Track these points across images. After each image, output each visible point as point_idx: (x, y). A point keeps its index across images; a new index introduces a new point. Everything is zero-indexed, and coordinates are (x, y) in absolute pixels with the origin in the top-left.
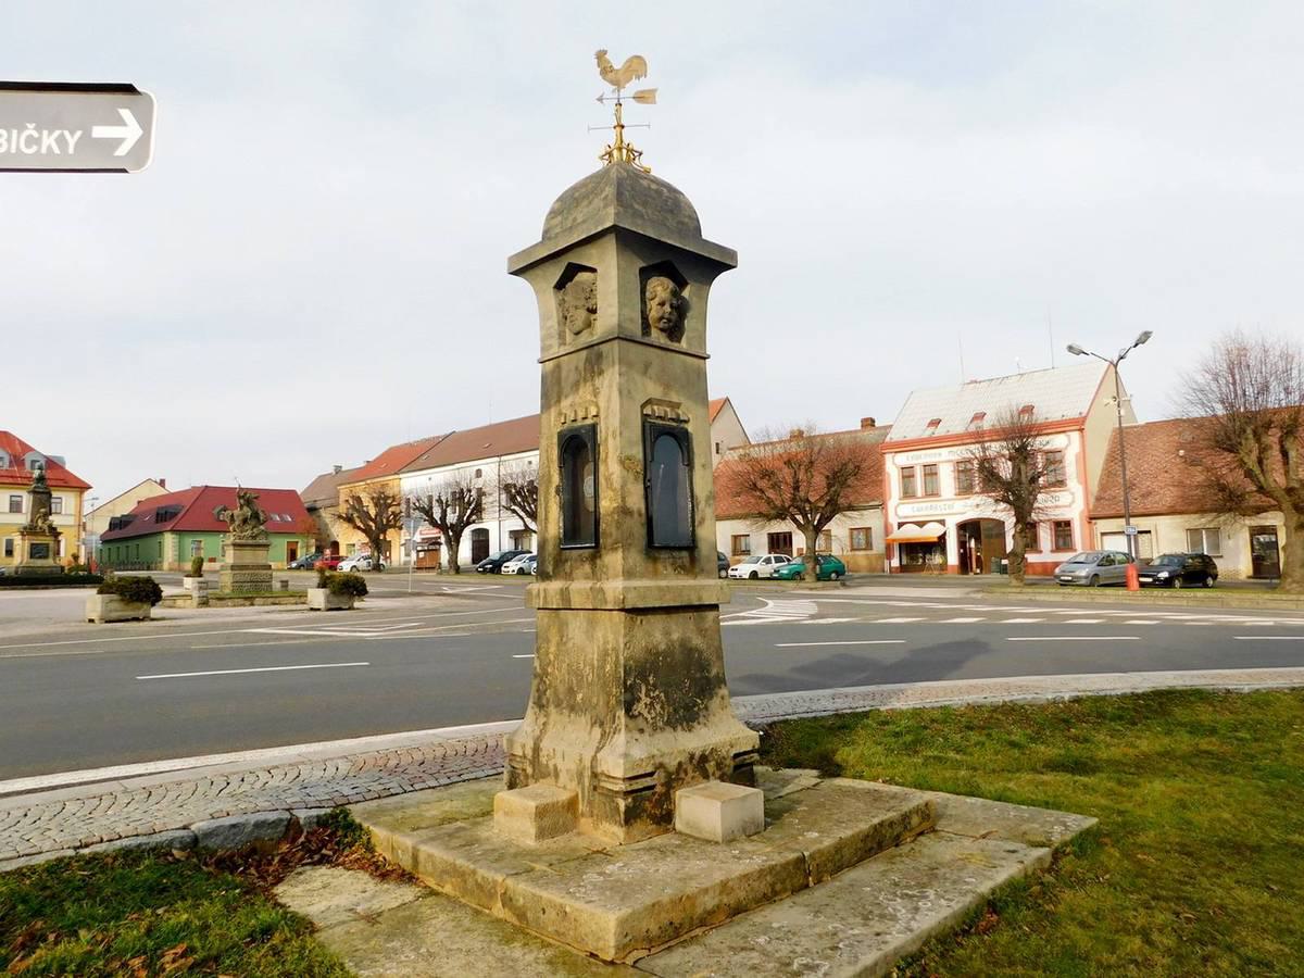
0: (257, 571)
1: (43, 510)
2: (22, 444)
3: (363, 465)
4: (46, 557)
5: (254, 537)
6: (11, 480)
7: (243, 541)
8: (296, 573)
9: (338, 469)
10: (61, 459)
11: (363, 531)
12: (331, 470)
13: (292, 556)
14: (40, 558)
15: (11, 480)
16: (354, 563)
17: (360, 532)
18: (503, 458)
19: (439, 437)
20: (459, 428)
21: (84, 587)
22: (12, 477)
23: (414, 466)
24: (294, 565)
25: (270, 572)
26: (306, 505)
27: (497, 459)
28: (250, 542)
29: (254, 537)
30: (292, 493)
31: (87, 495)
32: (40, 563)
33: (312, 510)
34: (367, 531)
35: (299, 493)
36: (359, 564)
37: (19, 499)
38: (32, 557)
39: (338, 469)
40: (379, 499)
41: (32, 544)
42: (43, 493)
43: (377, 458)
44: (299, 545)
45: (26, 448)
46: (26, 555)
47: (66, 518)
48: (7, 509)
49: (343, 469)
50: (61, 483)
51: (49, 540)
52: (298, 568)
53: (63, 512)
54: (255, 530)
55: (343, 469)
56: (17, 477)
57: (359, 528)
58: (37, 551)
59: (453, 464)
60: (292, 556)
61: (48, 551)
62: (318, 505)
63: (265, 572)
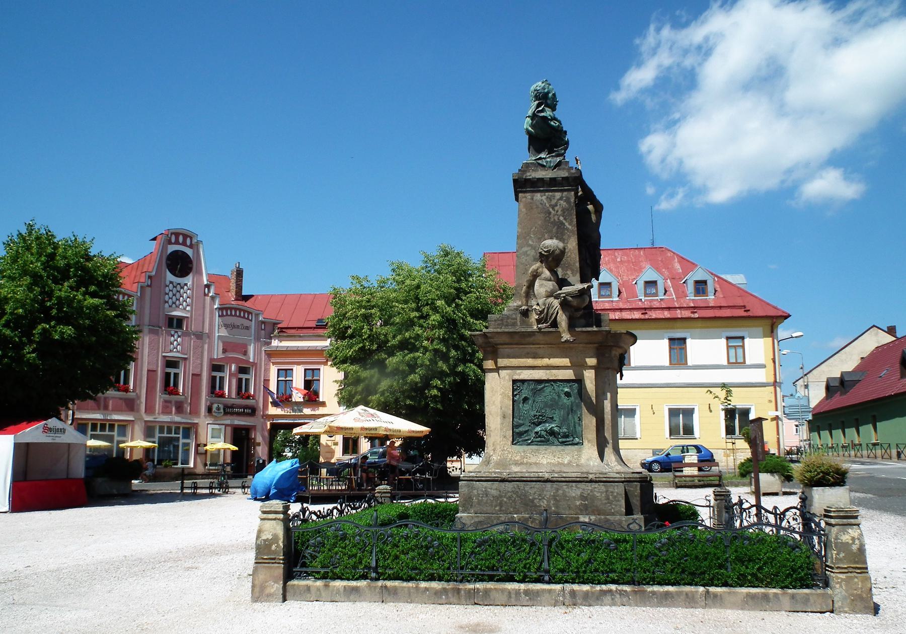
22: (669, 308)
50: (741, 313)
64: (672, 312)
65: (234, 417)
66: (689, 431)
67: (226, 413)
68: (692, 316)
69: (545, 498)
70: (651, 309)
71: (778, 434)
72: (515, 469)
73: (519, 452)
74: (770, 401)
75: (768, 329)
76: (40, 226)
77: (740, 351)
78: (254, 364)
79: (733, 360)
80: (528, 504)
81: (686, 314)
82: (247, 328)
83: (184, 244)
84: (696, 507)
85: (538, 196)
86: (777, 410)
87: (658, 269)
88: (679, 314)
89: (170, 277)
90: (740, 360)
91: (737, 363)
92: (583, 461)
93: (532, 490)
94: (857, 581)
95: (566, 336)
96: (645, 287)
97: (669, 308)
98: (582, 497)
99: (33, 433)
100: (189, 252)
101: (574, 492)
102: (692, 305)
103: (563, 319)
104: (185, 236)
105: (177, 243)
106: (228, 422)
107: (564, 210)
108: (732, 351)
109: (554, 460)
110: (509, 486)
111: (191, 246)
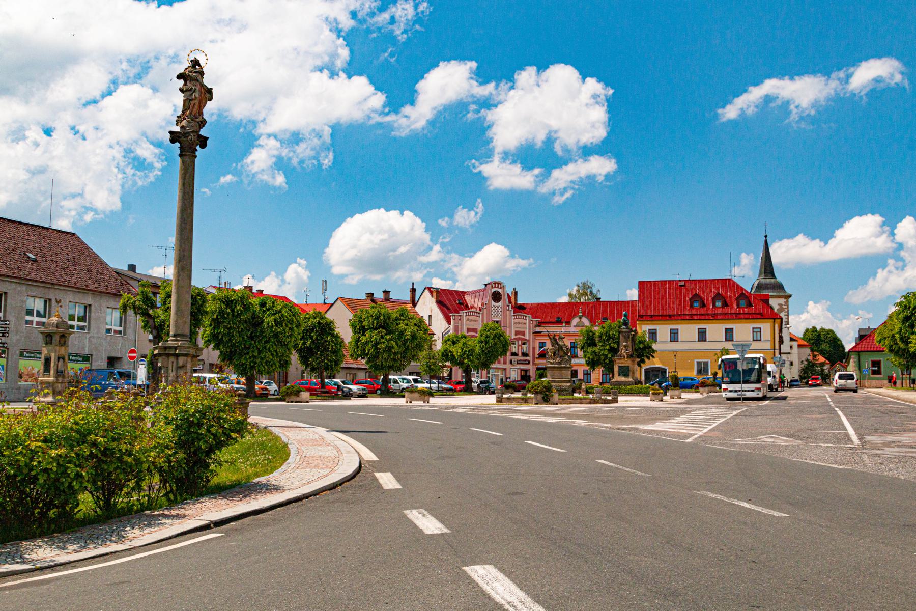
24: (142, 374)
53: (762, 339)
65: (521, 365)
67: (518, 363)
73: (619, 378)
76: (198, 58)
77: (759, 334)
78: (529, 341)
79: (755, 338)
82: (525, 324)
83: (498, 287)
84: (270, 428)
89: (493, 303)
90: (759, 338)
99: (173, 283)
100: (500, 291)
103: (626, 356)
104: (498, 284)
105: (495, 287)
106: (518, 367)
108: (755, 334)
111: (501, 288)
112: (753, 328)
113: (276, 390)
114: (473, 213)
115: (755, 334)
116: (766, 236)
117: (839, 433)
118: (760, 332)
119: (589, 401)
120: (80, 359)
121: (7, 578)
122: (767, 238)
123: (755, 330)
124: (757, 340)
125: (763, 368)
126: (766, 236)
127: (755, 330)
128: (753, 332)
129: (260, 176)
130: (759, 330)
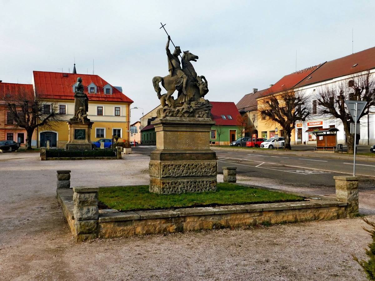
0: (195, 162)
1: (81, 108)
2: (103, 81)
3: (269, 87)
4: (84, 138)
5: (192, 114)
6: (97, 99)
7: (177, 119)
8: (236, 149)
9: (255, 90)
10: (120, 88)
11: (279, 122)
12: (252, 91)
13: (233, 138)
14: (80, 139)
15: (97, 99)
16: (270, 143)
17: (277, 123)
18: (371, 71)
19: (316, 66)
20: (329, 60)
21: (103, 159)
22: (98, 97)
23: (301, 84)
24: (234, 143)
25: (213, 162)
26: (239, 111)
27: (366, 72)
28: (186, 120)
29: (192, 114)
30: (232, 104)
31: (132, 106)
32: (80, 142)
33: (243, 113)
34: (282, 122)
35: (236, 104)
36: (273, 144)
37: (101, 109)
38: (75, 138)
39: (255, 90)
40: (289, 100)
41: (75, 130)
42: (81, 97)
43: (276, 84)
44: (236, 131)
45: (105, 83)
46: (73, 137)
47: (105, 117)
48: (96, 114)
49: (258, 90)
50: (120, 100)
51: (84, 127)
52: (236, 145)
53: (121, 115)
54: (193, 104)
55: (258, 90)
56: (100, 97)
57: (276, 120)
58: (78, 134)
59: (332, 79)
60: (233, 138)
61: (84, 134)
62: (245, 110)
63: (206, 162)
64: (99, 98)
66: (102, 136)
68: (105, 100)
69: (80, 147)
70: (92, 97)
71: (128, 137)
72: (75, 143)
74: (127, 127)
75: (128, 106)
77: (119, 111)
79: (117, 114)
80: (77, 148)
81: (103, 99)
85: (79, 99)
86: (128, 130)
87: (95, 83)
88: (101, 99)
90: (119, 114)
91: (117, 115)
92: (85, 142)
93: (78, 146)
94: (120, 156)
95: (84, 123)
96: (91, 89)
97: (98, 97)
98: (86, 147)
101: (84, 146)
102: (105, 96)
107: (83, 101)
108: (116, 111)
109: (81, 142)
110: (74, 146)
112: (115, 108)
113: (264, 147)
114: (150, 228)
115: (116, 111)
116: (75, 65)
117: (3, 92)
118: (120, 110)
119: (189, 74)
120: (263, 159)
121: (330, 149)
122: (75, 66)
123: (117, 109)
124: (118, 115)
125: (247, 211)
126: (75, 65)
127: (117, 109)
128: (115, 110)
129: (61, 112)
130: (119, 109)
